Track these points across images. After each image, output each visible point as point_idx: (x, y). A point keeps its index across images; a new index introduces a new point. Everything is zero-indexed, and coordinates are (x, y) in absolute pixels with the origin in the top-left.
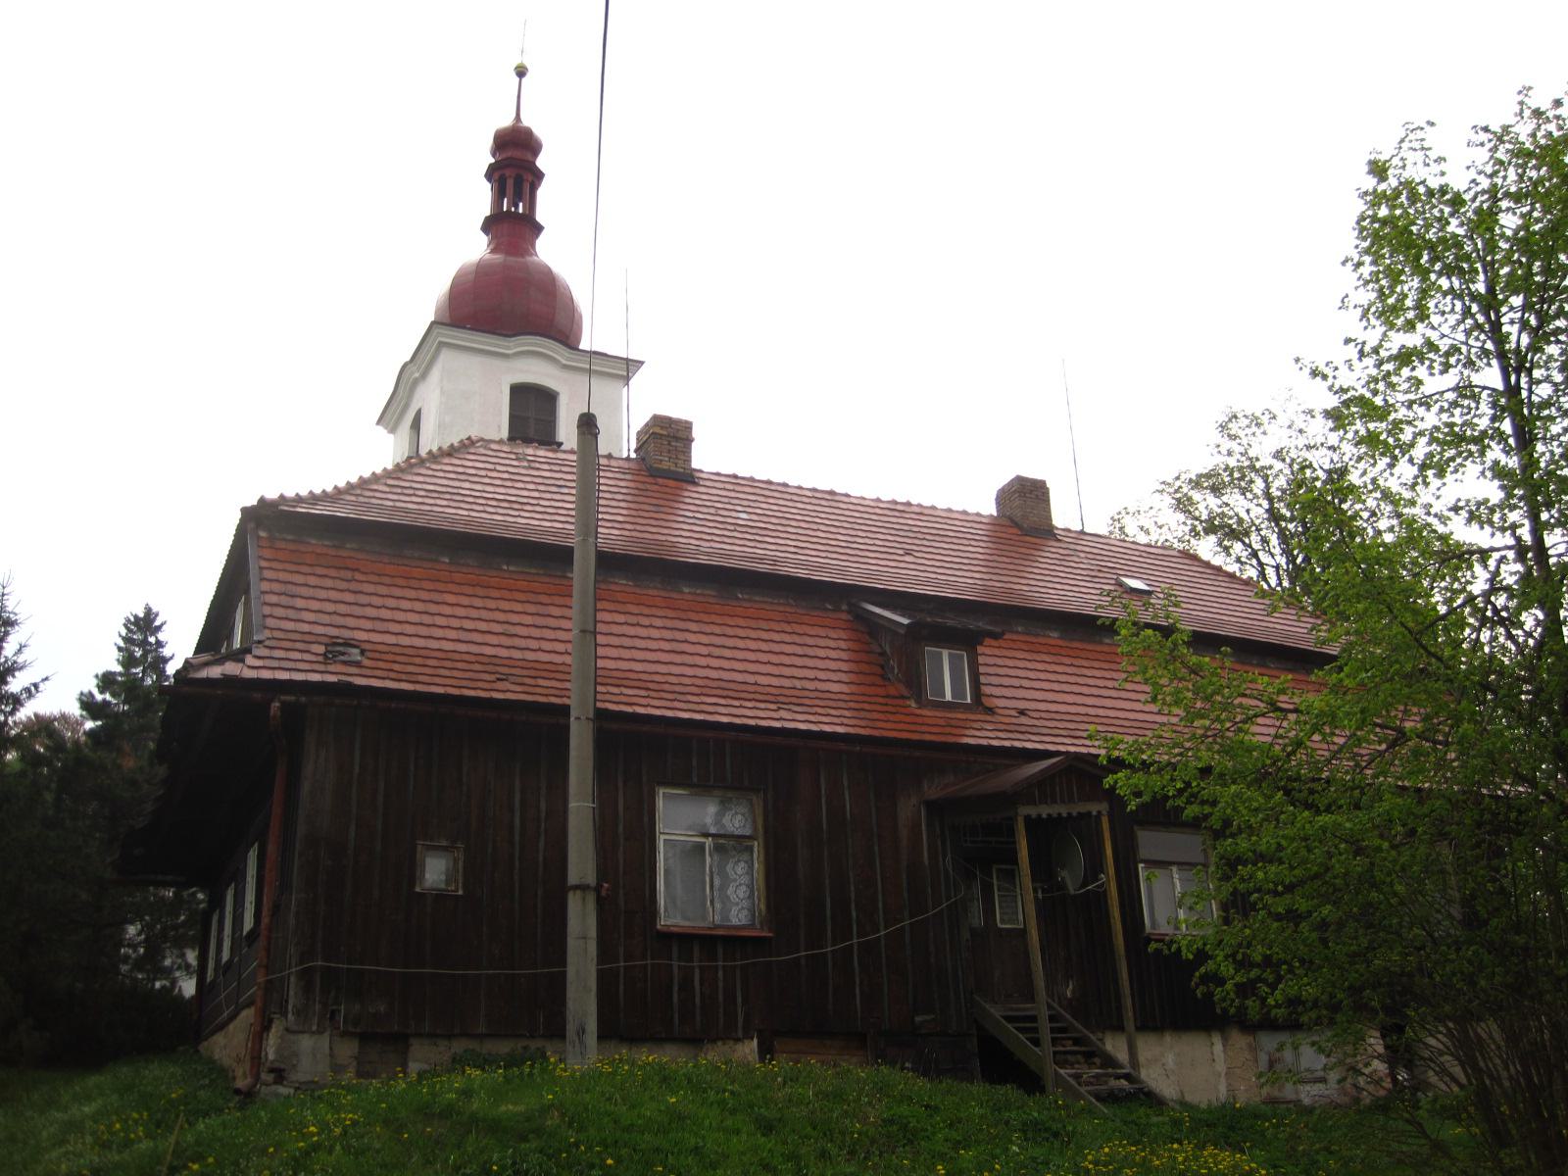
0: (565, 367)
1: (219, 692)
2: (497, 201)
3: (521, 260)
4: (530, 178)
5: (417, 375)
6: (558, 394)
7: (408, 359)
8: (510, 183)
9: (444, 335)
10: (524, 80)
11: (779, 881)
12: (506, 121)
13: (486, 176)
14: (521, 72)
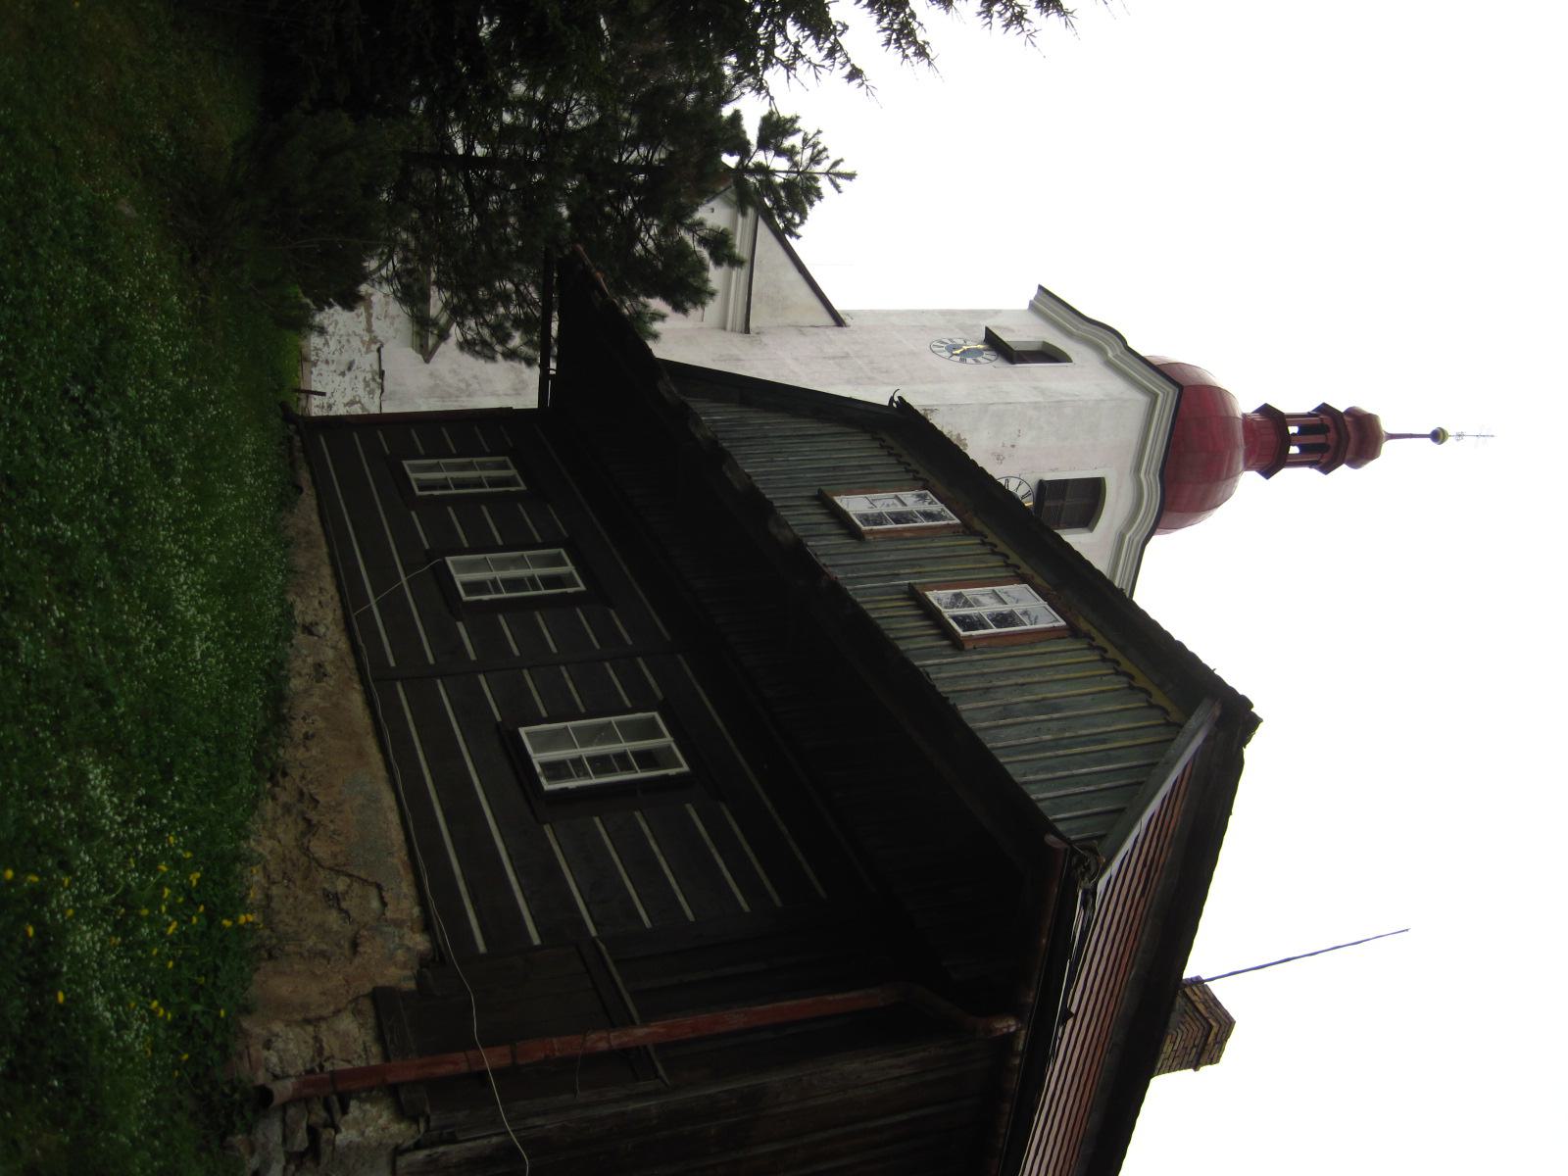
0: (1121, 537)
1: (1044, 941)
2: (1295, 418)
3: (1240, 457)
4: (1323, 461)
5: (1110, 355)
6: (1092, 530)
7: (1130, 344)
8: (1319, 439)
9: (1165, 401)
10: (1428, 440)
11: (447, 290)
12: (1387, 426)
13: (1324, 405)
14: (1438, 436)
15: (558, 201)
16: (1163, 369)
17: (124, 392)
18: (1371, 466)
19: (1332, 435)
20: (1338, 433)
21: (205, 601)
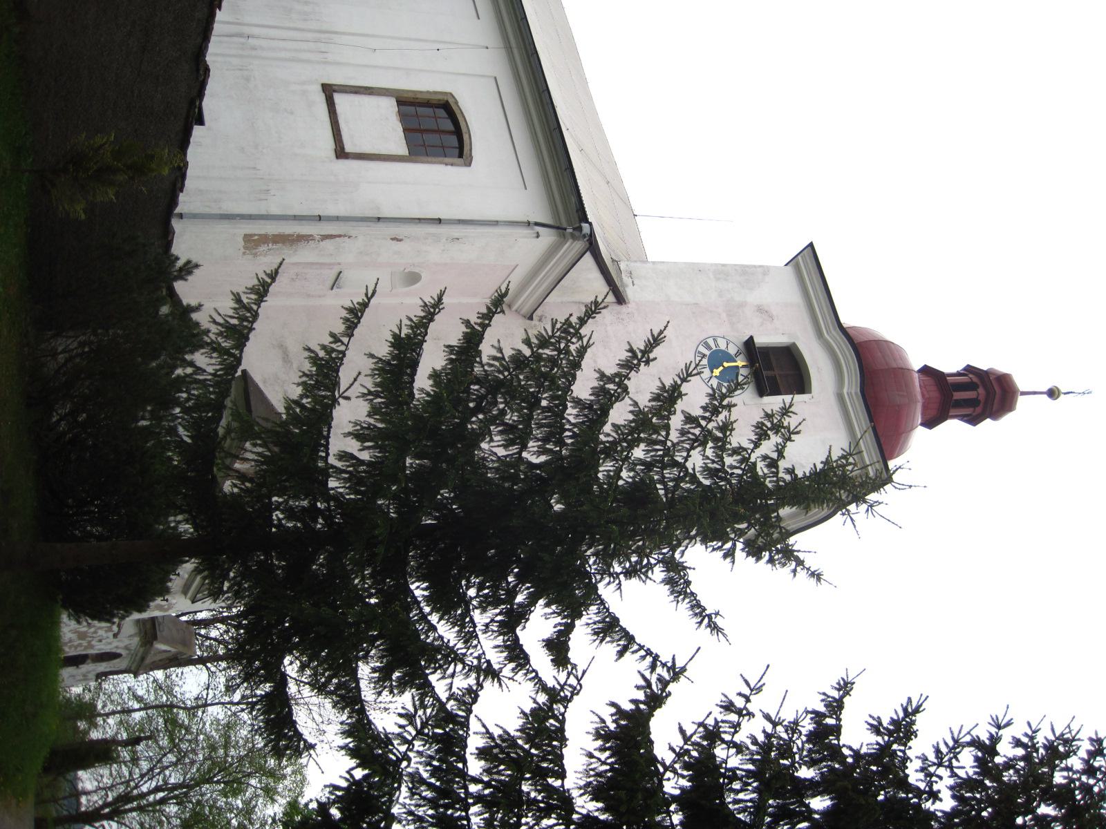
10: (1045, 396)
12: (1021, 383)
13: (968, 366)
14: (1053, 393)
15: (548, 596)
16: (848, 331)
17: (166, 722)
18: (1008, 418)
19: (981, 390)
20: (985, 387)
21: (320, 521)
